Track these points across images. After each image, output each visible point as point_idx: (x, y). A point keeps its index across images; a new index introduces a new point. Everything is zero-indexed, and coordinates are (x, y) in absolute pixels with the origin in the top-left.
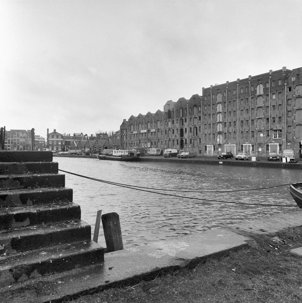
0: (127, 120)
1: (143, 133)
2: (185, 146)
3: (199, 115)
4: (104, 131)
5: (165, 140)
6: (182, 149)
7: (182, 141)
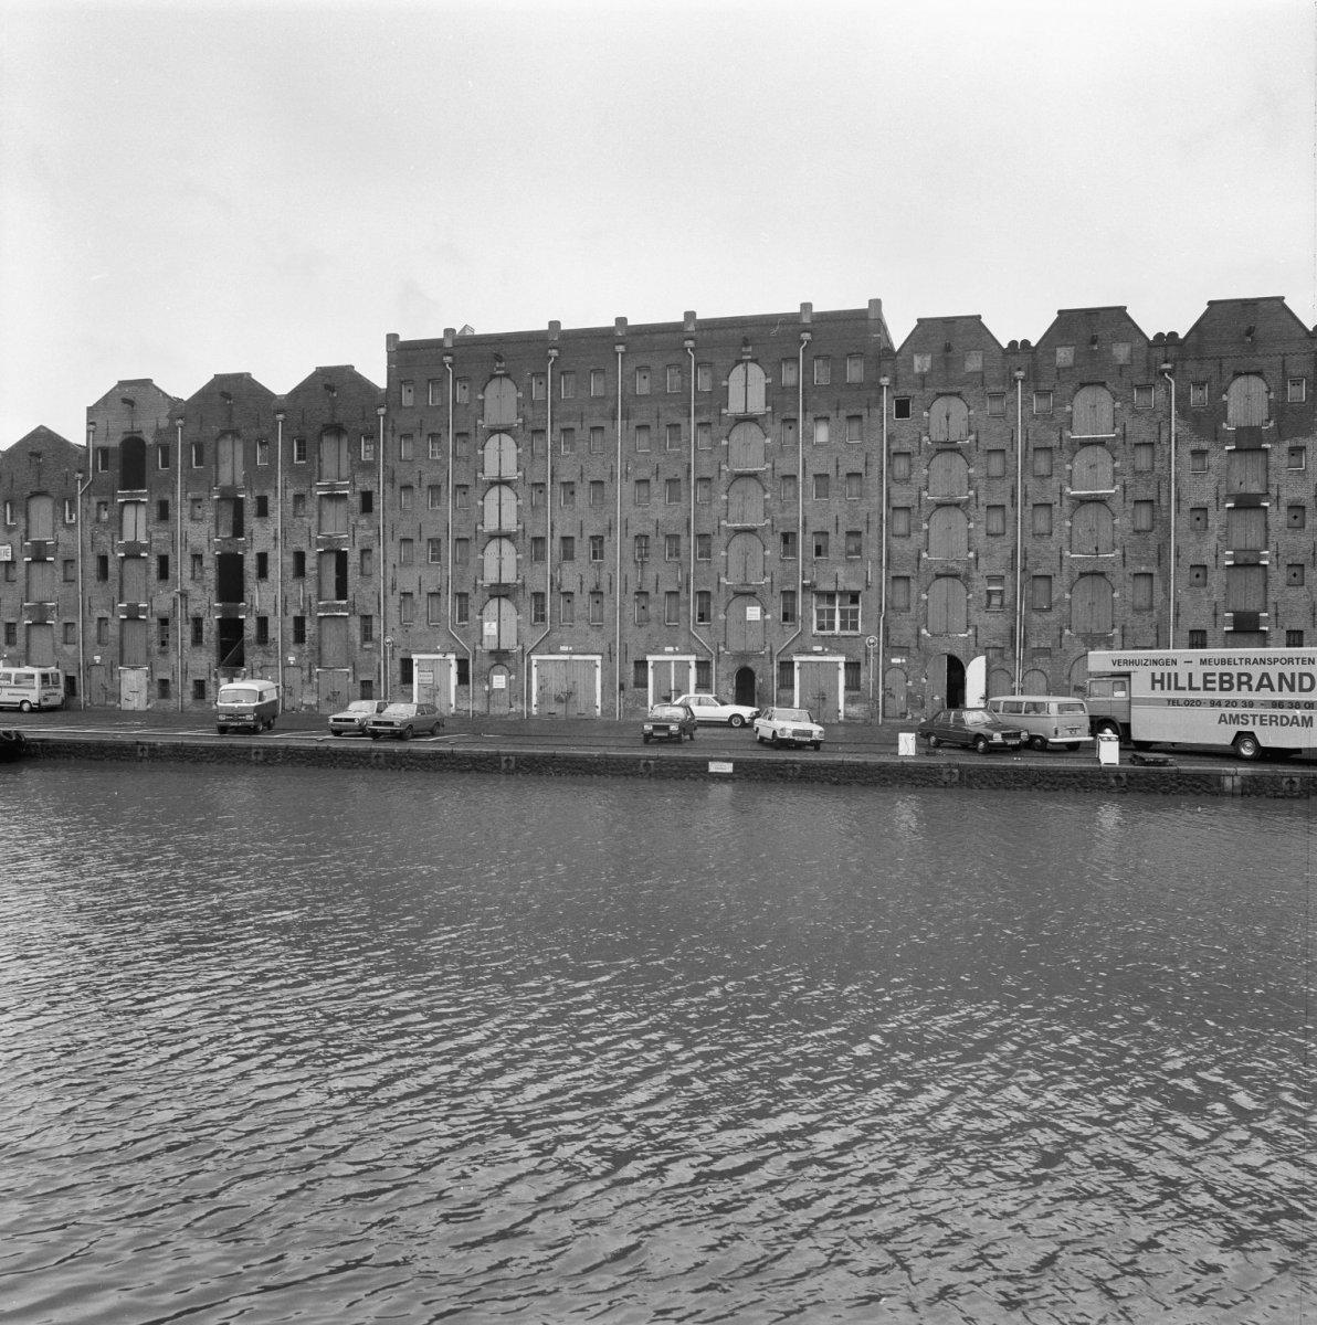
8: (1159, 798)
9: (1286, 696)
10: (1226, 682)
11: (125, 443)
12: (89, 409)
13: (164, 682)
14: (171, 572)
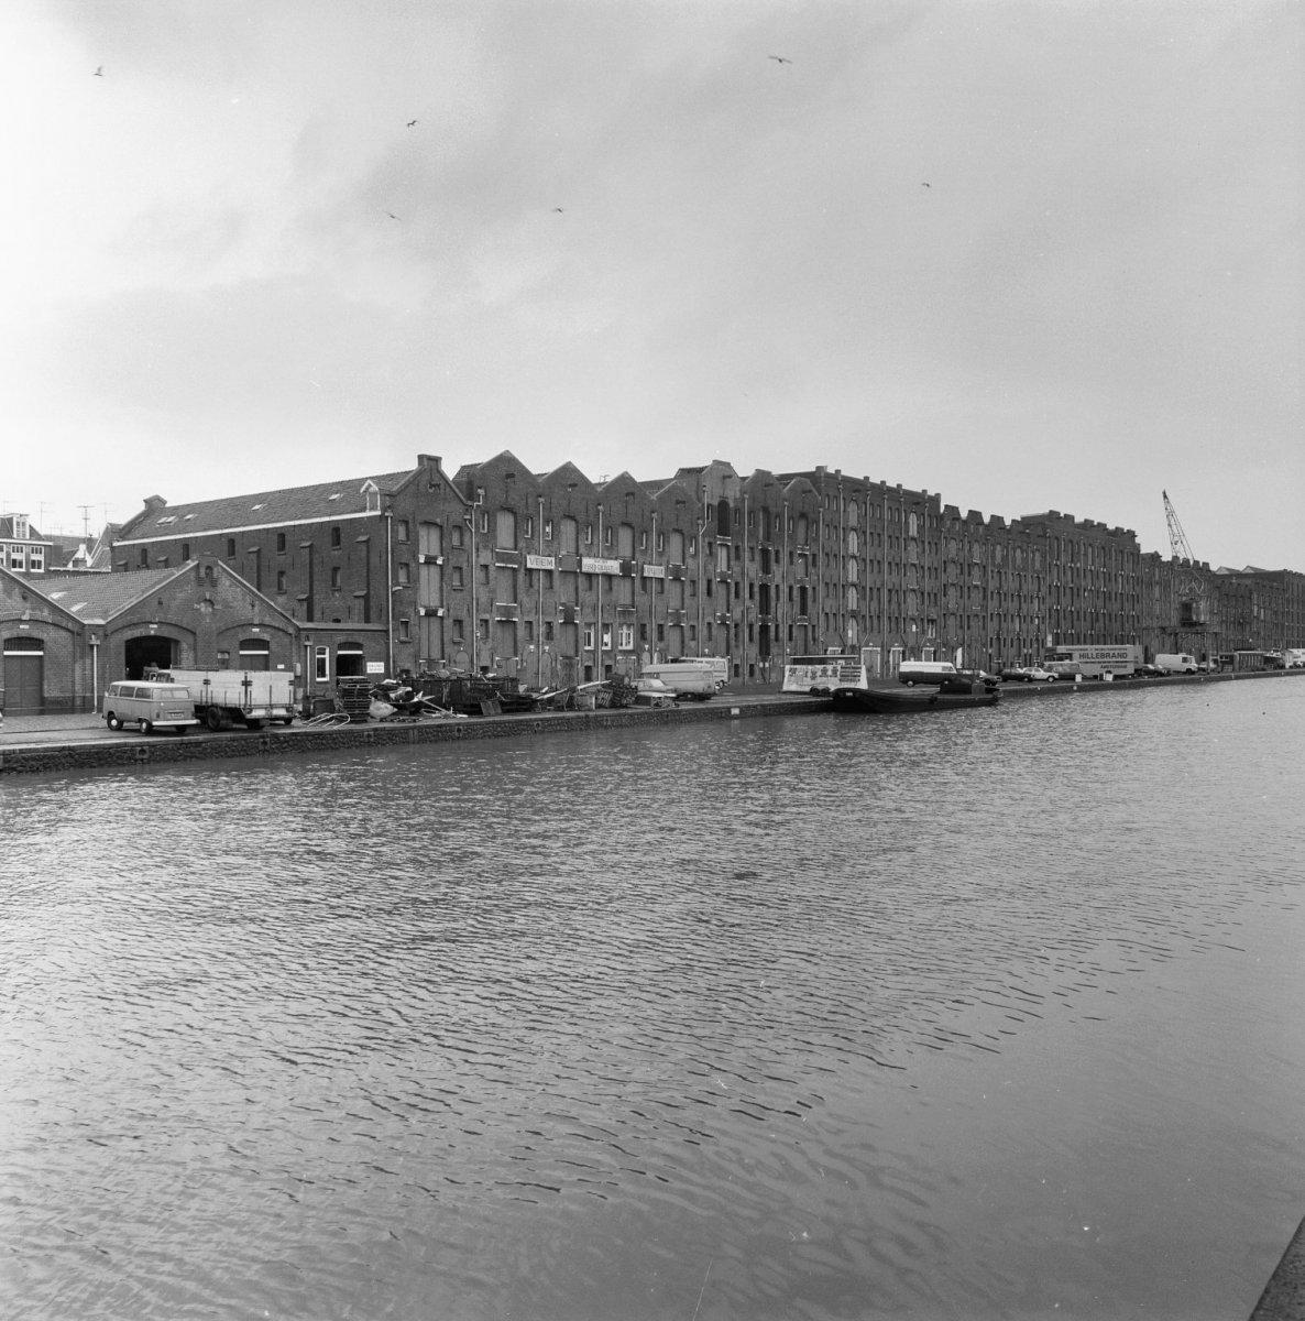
0: (450, 470)
1: (589, 576)
2: (774, 650)
3: (814, 549)
4: (1120, 526)
5: (707, 620)
6: (764, 660)
7: (764, 629)
8: (54, 774)
9: (1119, 659)
10: (1103, 656)
11: (719, 504)
12: (1132, 535)
13: (736, 666)
14: (742, 594)
